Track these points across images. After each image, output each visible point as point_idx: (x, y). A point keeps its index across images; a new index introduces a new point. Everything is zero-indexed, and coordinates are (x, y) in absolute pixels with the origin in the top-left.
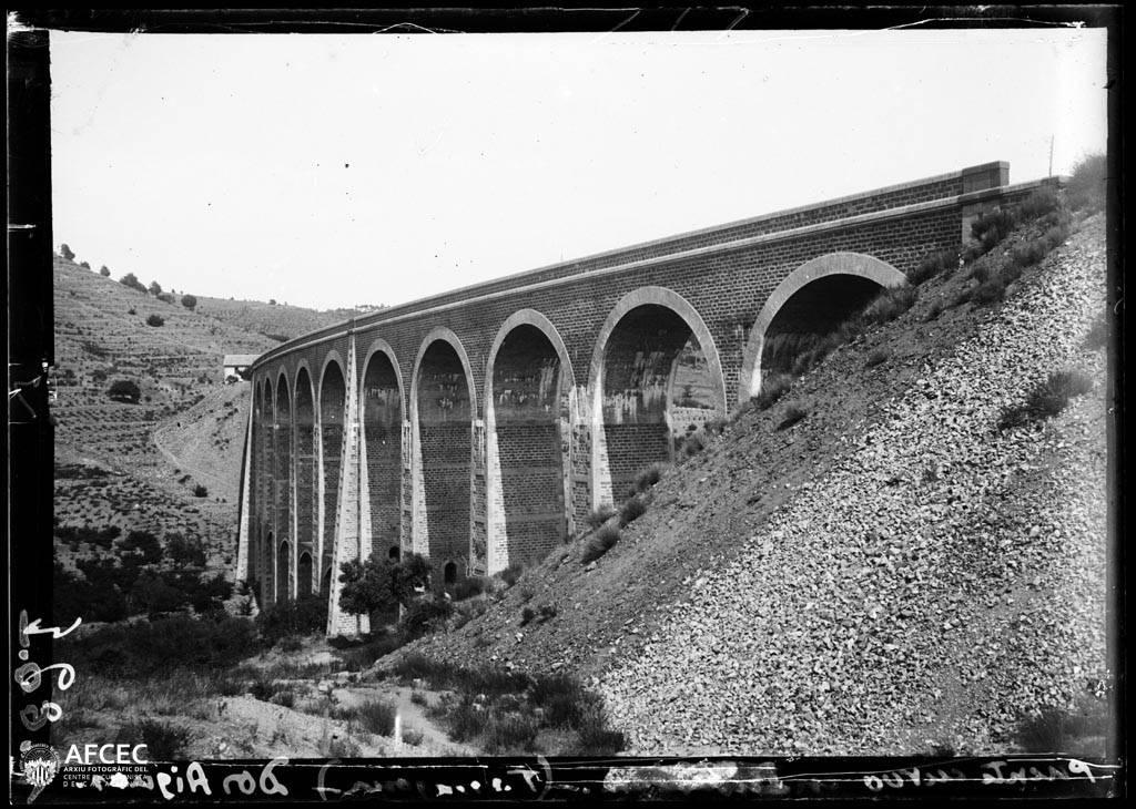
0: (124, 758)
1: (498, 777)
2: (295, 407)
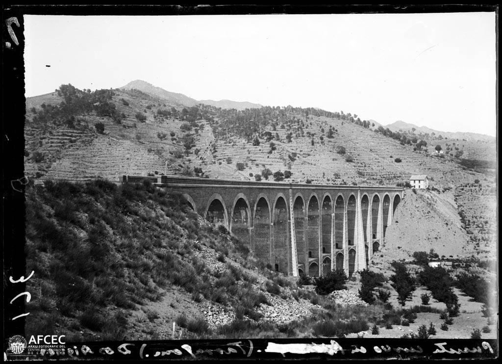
0: (54, 341)
1: (131, 352)
2: (383, 201)
